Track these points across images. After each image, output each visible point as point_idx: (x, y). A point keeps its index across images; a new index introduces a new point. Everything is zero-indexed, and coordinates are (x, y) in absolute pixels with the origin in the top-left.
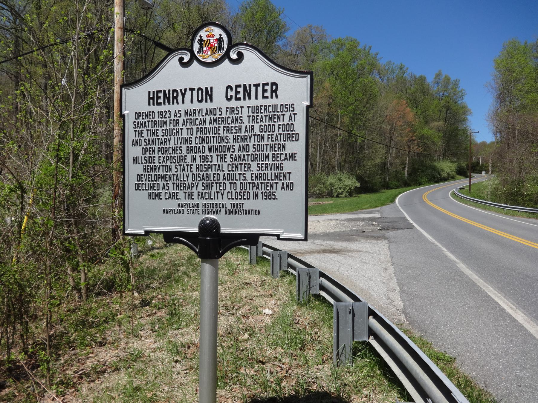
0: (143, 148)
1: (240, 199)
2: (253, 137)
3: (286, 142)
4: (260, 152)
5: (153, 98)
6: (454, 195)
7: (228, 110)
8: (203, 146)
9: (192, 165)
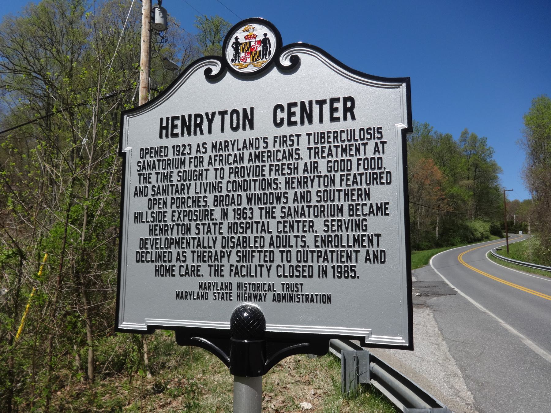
0: (150, 199)
1: (298, 277)
2: (316, 180)
3: (371, 187)
4: (329, 203)
5: (166, 128)
6: (491, 256)
7: (278, 140)
8: (239, 195)
9: (222, 224)
